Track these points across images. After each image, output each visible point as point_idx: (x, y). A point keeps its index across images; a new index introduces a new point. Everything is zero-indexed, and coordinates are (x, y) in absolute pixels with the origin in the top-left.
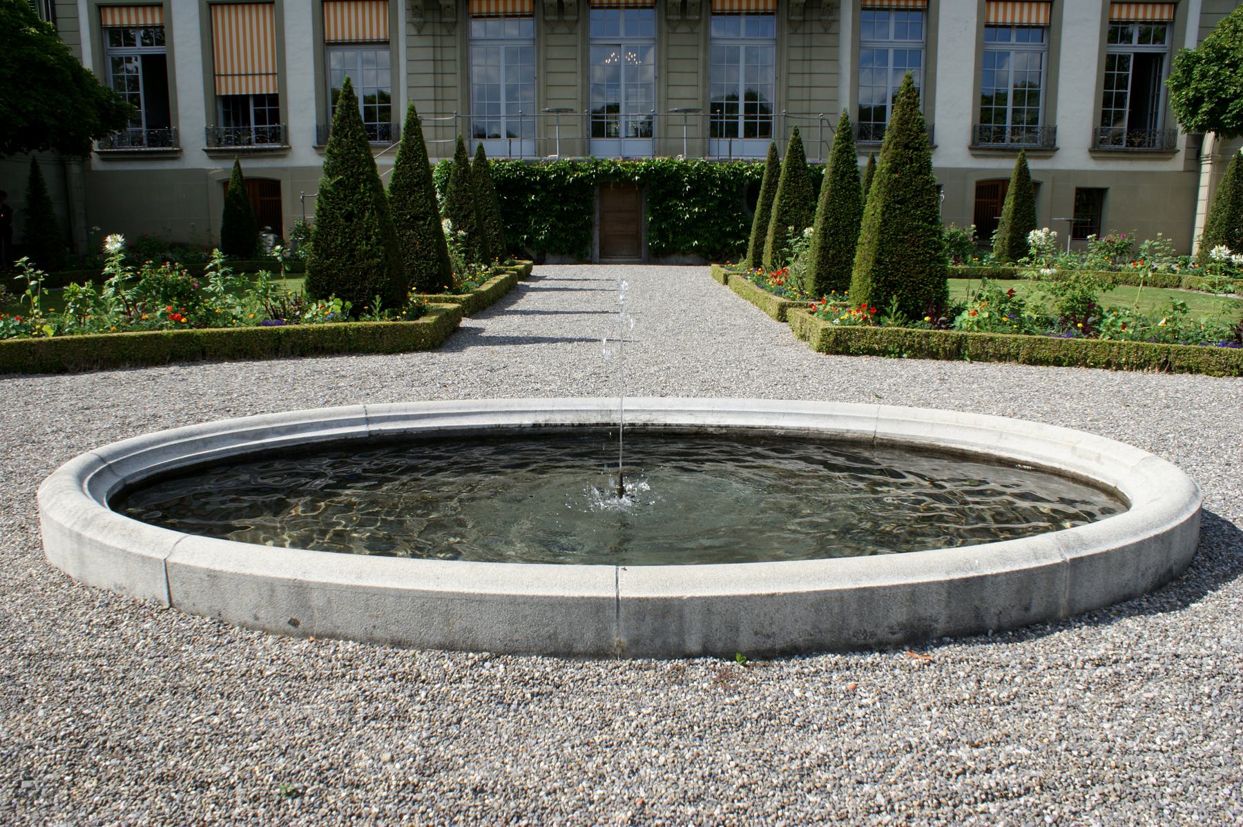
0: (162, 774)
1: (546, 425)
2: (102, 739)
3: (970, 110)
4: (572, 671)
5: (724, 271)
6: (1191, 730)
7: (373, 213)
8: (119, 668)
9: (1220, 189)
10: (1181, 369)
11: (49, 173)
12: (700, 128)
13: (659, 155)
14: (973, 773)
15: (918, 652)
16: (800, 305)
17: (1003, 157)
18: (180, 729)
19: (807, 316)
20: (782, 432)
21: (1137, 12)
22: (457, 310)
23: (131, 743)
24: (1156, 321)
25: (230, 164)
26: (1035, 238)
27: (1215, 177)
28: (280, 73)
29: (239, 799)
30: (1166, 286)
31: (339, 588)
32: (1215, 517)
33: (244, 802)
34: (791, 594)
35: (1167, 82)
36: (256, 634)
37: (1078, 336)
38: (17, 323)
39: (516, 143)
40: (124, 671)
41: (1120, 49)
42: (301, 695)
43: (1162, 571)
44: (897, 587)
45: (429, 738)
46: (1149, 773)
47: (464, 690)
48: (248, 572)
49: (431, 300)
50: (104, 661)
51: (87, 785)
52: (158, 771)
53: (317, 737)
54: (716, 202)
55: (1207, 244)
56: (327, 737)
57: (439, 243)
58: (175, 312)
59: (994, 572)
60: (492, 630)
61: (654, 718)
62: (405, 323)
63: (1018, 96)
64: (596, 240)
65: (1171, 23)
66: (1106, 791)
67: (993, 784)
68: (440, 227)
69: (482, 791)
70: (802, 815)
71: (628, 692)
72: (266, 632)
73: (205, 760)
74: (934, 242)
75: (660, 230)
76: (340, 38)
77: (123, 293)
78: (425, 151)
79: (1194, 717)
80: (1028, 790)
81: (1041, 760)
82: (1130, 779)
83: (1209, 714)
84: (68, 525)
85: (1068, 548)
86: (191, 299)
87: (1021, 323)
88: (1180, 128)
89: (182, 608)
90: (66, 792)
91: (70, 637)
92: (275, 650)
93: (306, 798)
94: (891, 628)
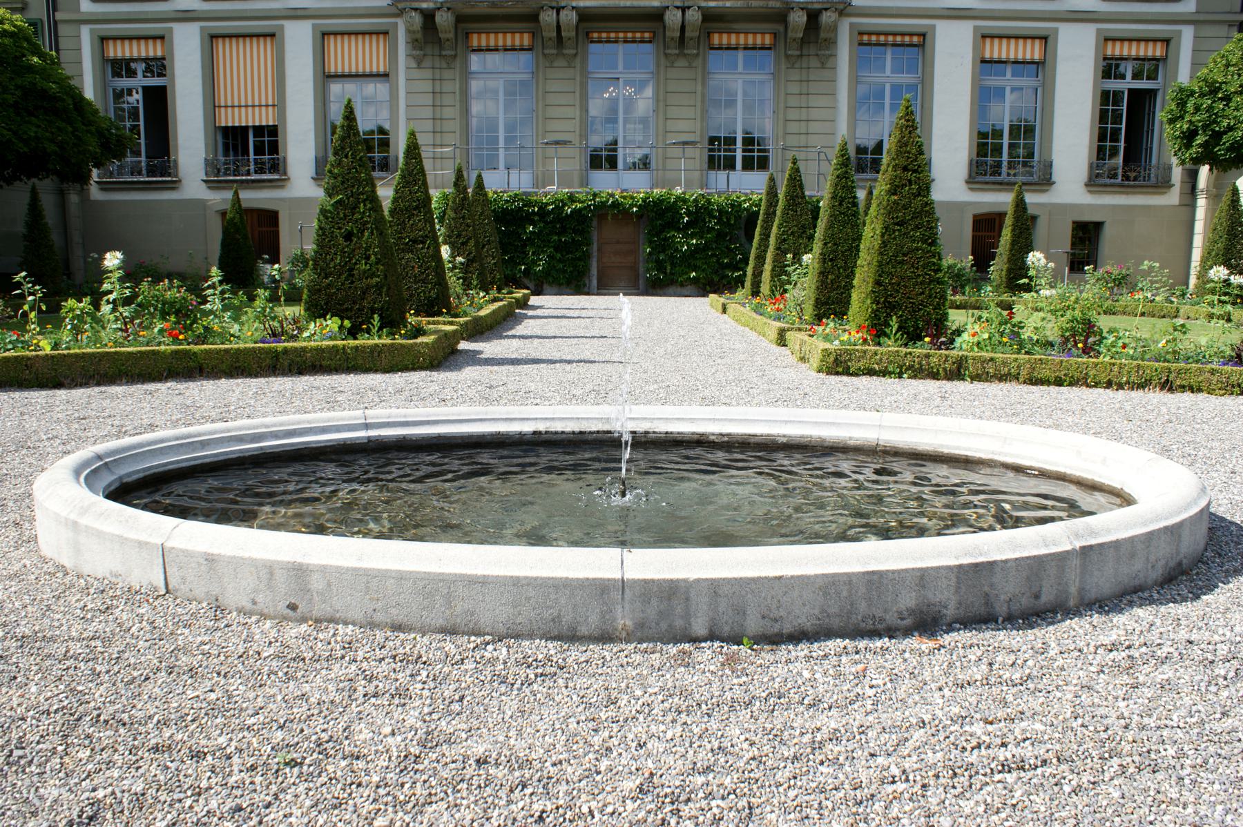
0: (157, 744)
1: (547, 432)
2: (95, 713)
3: (966, 144)
4: (575, 653)
5: (722, 300)
6: (1209, 708)
7: (372, 233)
8: (114, 651)
9: (1216, 220)
10: (1183, 388)
11: (48, 202)
12: (698, 161)
13: (657, 187)
14: (989, 747)
15: (928, 638)
16: (800, 330)
17: (1000, 190)
18: (176, 705)
19: (807, 338)
20: (784, 440)
21: (1130, 49)
22: (455, 332)
23: (125, 717)
24: (1157, 342)
25: (228, 195)
26: (1034, 260)
27: (1210, 210)
28: (280, 105)
29: (236, 768)
30: (1164, 317)
31: (339, 570)
32: (1223, 519)
33: (241, 771)
34: (798, 577)
35: (1161, 115)
36: (254, 618)
37: (1078, 356)
38: (15, 337)
39: (514, 175)
40: (119, 652)
41: (1113, 85)
42: (299, 675)
43: (1172, 564)
44: (906, 571)
45: (430, 714)
46: (1167, 746)
47: (466, 671)
48: (246, 555)
49: (429, 323)
50: (99, 643)
51: (80, 755)
52: (153, 742)
53: (316, 712)
54: (714, 234)
55: (1205, 266)
56: (326, 712)
57: (437, 266)
58: (173, 329)
59: (1004, 558)
60: (494, 613)
61: (660, 698)
62: (404, 341)
63: (1015, 130)
64: (594, 271)
65: (1164, 59)
66: (1124, 763)
67: (1009, 756)
68: (440, 251)
69: (486, 762)
70: (814, 785)
71: (634, 674)
72: (264, 616)
73: (201, 732)
74: (934, 264)
75: (658, 262)
76: (340, 70)
77: (121, 309)
78: (425, 183)
79: (1211, 697)
80: (1044, 762)
81: (1057, 735)
82: (1148, 752)
83: (1225, 693)
84: (64, 514)
85: (1077, 536)
86: (188, 316)
87: (1021, 344)
88: (1175, 161)
89: (178, 594)
90: (58, 760)
91: (64, 621)
92: (274, 633)
93: (305, 768)
94: (900, 613)
